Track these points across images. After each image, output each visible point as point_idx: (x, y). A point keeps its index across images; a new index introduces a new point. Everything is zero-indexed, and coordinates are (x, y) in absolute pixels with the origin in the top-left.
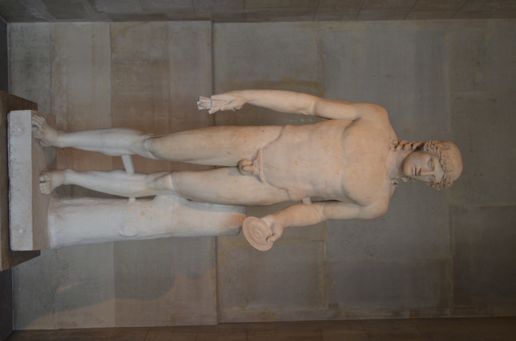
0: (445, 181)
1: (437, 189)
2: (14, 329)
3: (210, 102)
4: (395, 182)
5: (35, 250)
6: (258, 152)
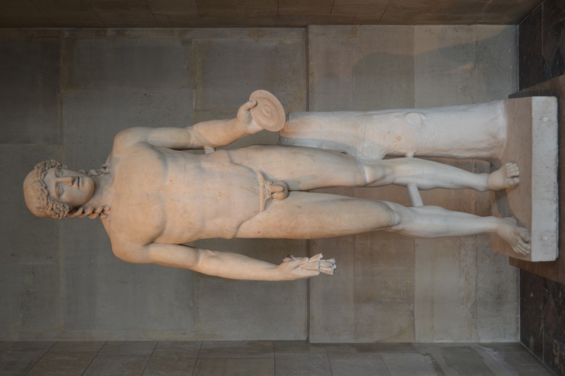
0: (44, 169)
1: (55, 161)
2: (518, 26)
3: (320, 268)
4: (105, 170)
5: (529, 98)
6: (265, 208)
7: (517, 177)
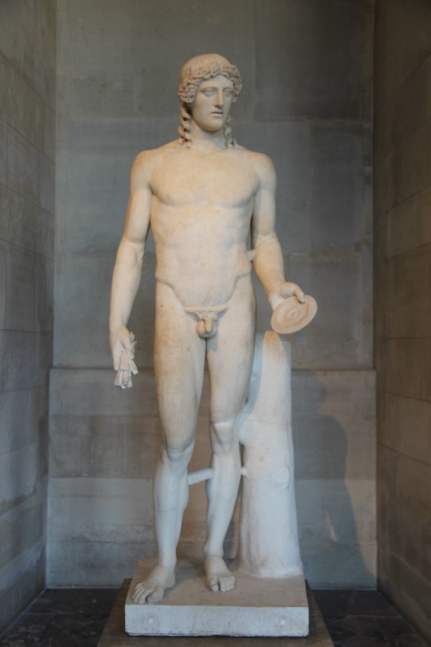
3: (122, 372)
5: (307, 603)
7: (219, 589)
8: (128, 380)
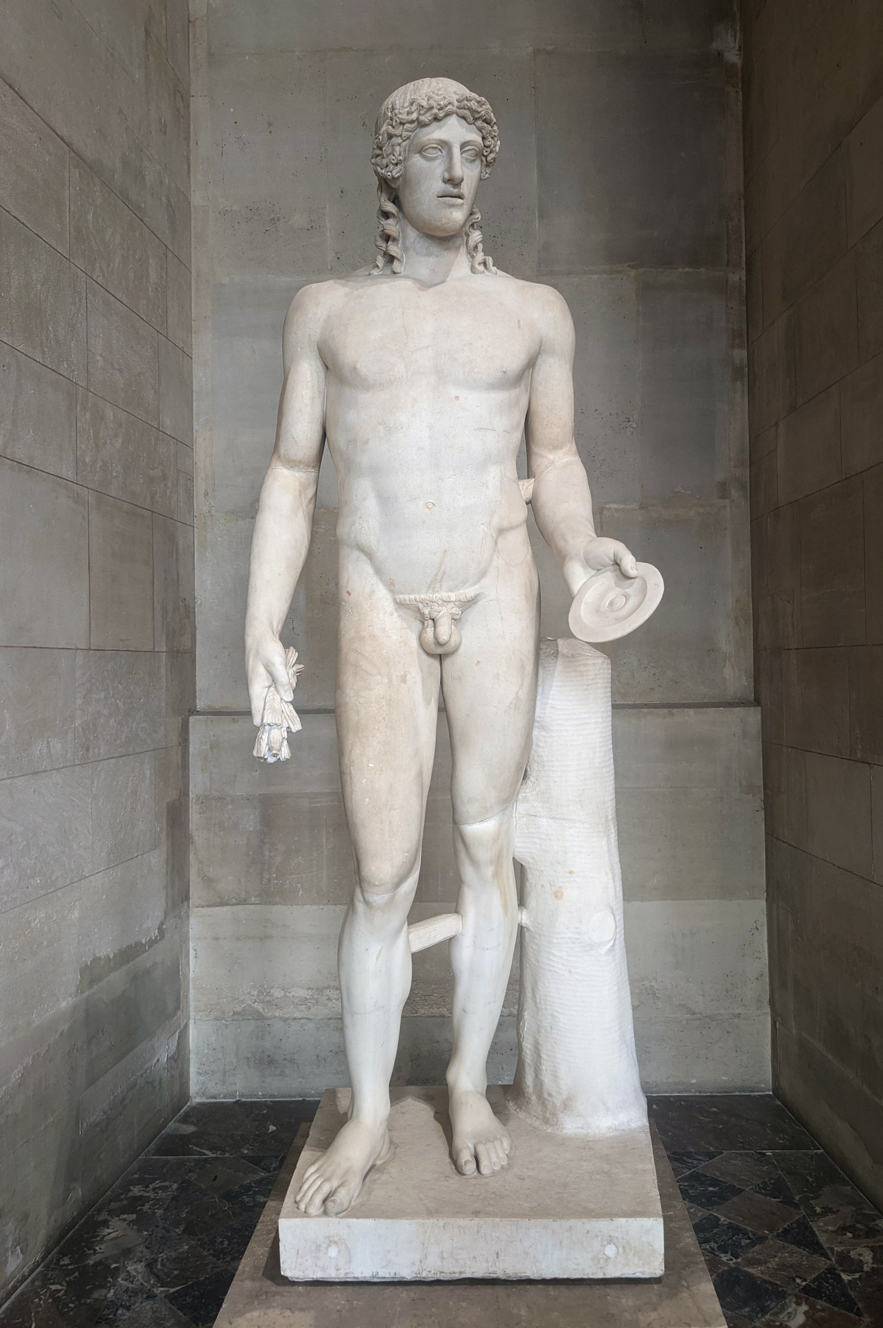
0: (477, 116)
2: (771, 1093)
3: (267, 728)
8: (281, 745)
